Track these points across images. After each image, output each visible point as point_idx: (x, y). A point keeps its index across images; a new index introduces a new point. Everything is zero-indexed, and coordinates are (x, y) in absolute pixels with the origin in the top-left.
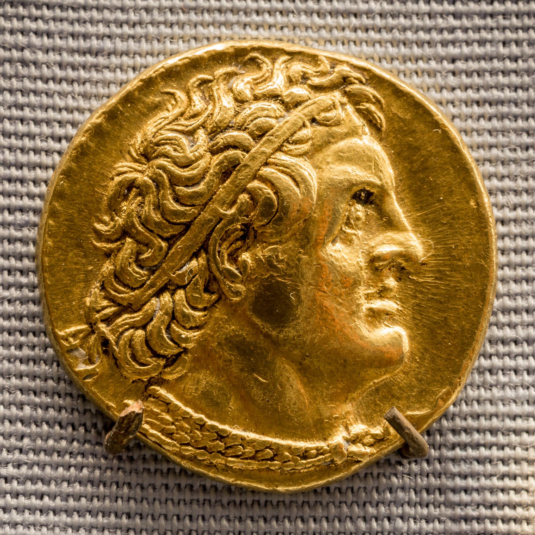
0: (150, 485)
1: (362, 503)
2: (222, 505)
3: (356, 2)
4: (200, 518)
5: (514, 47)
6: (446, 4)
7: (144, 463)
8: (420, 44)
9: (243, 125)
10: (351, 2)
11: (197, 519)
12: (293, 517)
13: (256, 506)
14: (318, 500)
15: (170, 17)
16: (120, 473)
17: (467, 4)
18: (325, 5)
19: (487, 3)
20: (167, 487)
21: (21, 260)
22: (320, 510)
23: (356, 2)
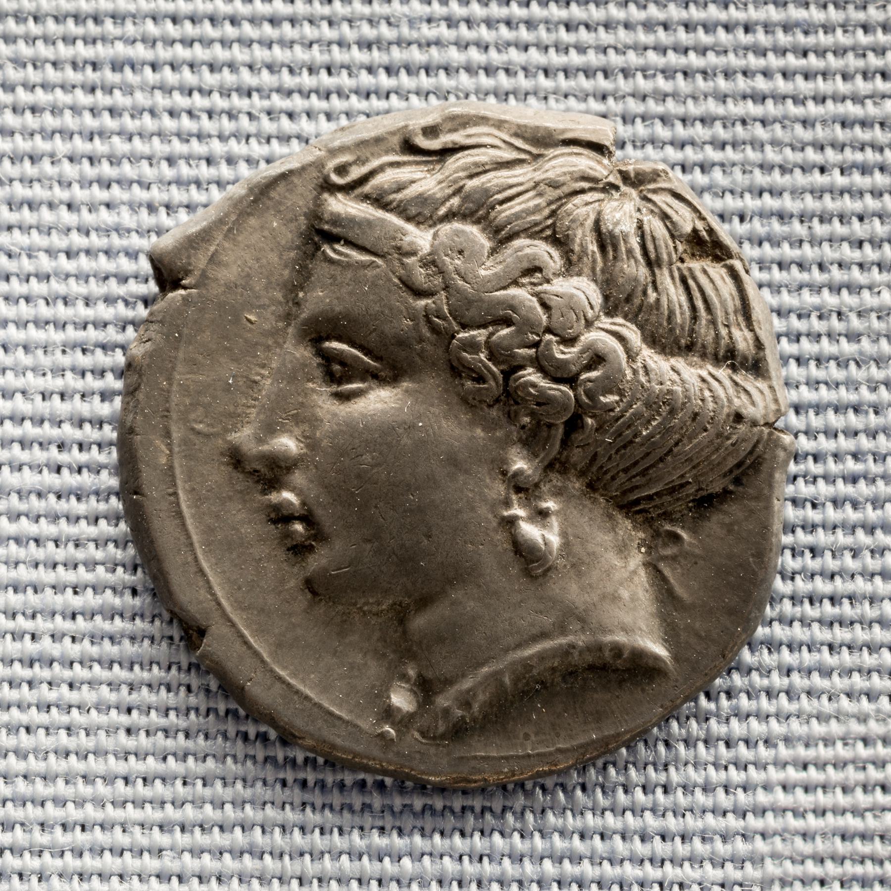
0: (556, 785)
1: (540, 810)
2: (393, 813)
3: (429, 3)
4: (336, 830)
5: (186, 72)
6: (514, 6)
7: (265, 746)
8: (668, 73)
9: (480, 206)
10: (321, 3)
11: (331, 832)
12: (468, 830)
13: (428, 813)
14: (327, 802)
15: (33, 28)
16: (249, 763)
17: (645, 7)
18: (476, 10)
19: (520, 4)
20: (284, 783)
21: (80, 426)
22: (510, 818)
23: (429, 3)
